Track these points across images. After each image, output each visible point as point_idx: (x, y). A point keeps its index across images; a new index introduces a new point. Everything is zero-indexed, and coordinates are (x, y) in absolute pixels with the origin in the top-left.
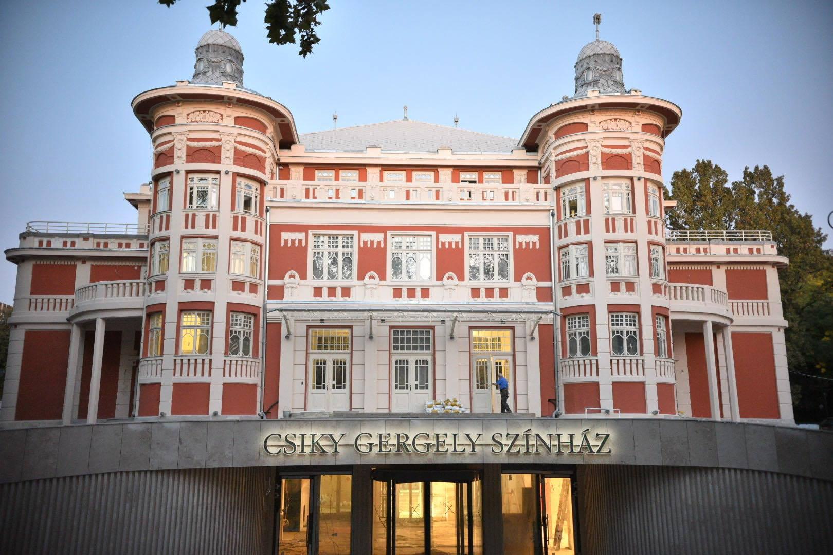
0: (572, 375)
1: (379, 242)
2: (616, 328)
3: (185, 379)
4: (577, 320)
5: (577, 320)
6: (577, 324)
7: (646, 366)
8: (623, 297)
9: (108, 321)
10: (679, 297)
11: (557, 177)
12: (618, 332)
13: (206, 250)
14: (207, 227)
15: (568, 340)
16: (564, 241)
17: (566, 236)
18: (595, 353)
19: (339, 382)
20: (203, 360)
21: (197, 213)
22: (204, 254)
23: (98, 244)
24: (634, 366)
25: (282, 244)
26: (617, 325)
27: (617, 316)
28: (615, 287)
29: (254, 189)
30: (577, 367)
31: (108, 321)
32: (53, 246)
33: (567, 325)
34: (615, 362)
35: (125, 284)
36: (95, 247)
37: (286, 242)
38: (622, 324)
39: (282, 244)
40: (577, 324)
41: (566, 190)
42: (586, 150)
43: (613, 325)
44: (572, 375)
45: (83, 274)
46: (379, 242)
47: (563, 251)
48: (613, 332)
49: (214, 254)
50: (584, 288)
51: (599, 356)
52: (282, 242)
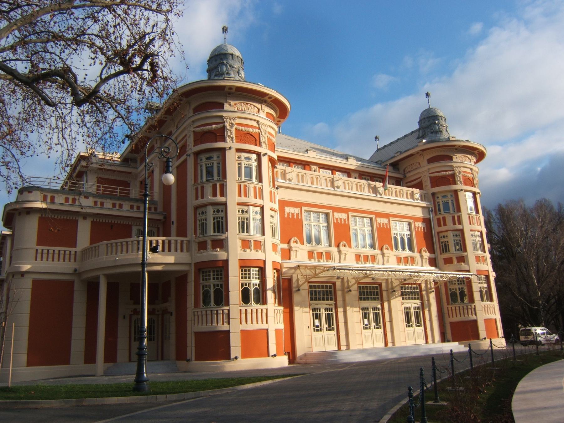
0: (204, 324)
1: (345, 220)
2: (244, 281)
3: (249, 326)
4: (212, 274)
5: (212, 274)
6: (212, 277)
7: (477, 309)
8: (252, 254)
9: (107, 276)
10: (179, 250)
11: (194, 146)
12: (246, 285)
13: (217, 215)
14: (454, 224)
15: (202, 292)
16: (201, 201)
17: (202, 197)
18: (228, 304)
19: (329, 326)
20: (246, 310)
21: (205, 185)
22: (214, 219)
23: (96, 203)
24: (249, 316)
25: (286, 216)
26: (246, 278)
27: (245, 271)
28: (246, 244)
29: (449, 196)
30: (200, 317)
31: (107, 276)
32: (56, 201)
33: (201, 278)
34: (244, 311)
35: (122, 243)
36: (63, 202)
37: (288, 214)
38: (210, 279)
39: (286, 216)
40: (212, 277)
41: (203, 157)
42: (222, 125)
43: (242, 278)
44: (204, 324)
45: (84, 232)
46: (297, 215)
47: (200, 211)
48: (242, 285)
49: (206, 220)
50: (259, 245)
51: (231, 307)
52: (286, 214)
